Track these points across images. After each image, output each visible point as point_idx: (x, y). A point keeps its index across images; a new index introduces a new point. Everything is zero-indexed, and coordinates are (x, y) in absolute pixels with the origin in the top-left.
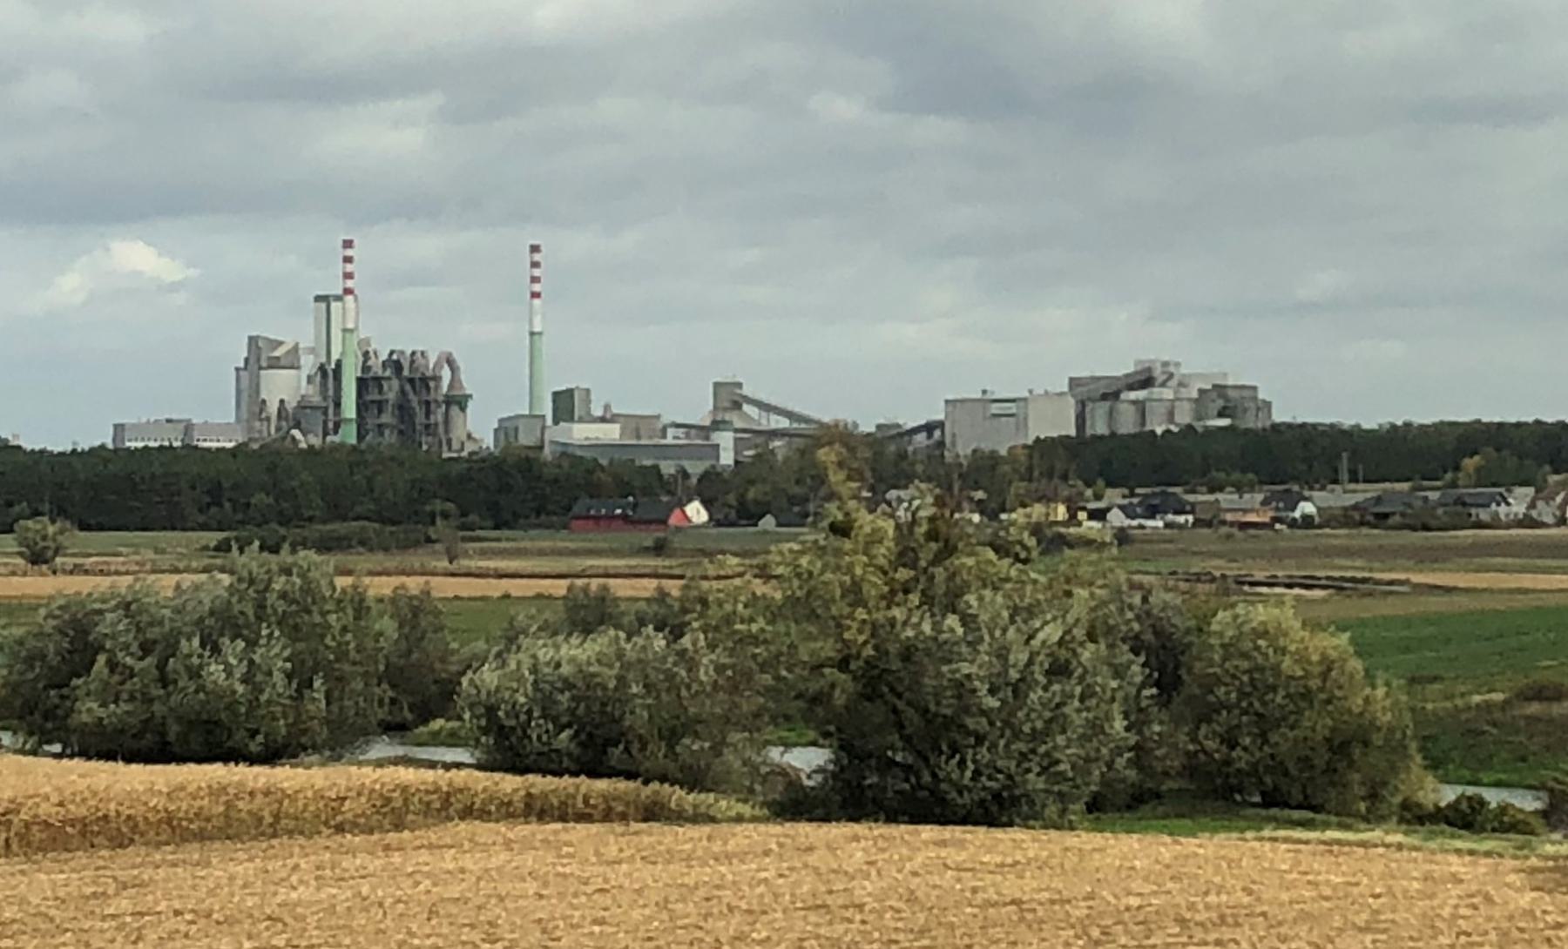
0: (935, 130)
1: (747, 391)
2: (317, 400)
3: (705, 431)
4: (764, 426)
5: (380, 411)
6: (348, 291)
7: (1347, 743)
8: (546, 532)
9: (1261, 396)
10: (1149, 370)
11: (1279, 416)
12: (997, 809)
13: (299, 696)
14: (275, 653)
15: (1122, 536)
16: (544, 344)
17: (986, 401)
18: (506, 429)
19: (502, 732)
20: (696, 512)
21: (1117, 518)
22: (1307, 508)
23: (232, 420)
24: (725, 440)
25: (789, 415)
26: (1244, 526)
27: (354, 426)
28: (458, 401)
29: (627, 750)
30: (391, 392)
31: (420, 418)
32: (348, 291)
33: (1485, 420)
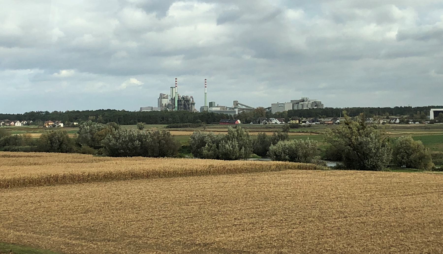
0: (262, 61)
1: (239, 102)
2: (171, 104)
3: (233, 109)
4: (241, 108)
6: (176, 86)
7: (422, 157)
12: (374, 168)
13: (240, 150)
14: (236, 143)
15: (309, 126)
16: (207, 95)
17: (278, 104)
18: (202, 108)
19: (276, 155)
20: (239, 121)
21: (307, 122)
22: (338, 121)
23: (157, 107)
24: (236, 110)
25: (246, 106)
26: (328, 124)
27: (177, 108)
28: (193, 104)
29: (298, 159)
30: (183, 102)
31: (187, 107)
32: (176, 86)
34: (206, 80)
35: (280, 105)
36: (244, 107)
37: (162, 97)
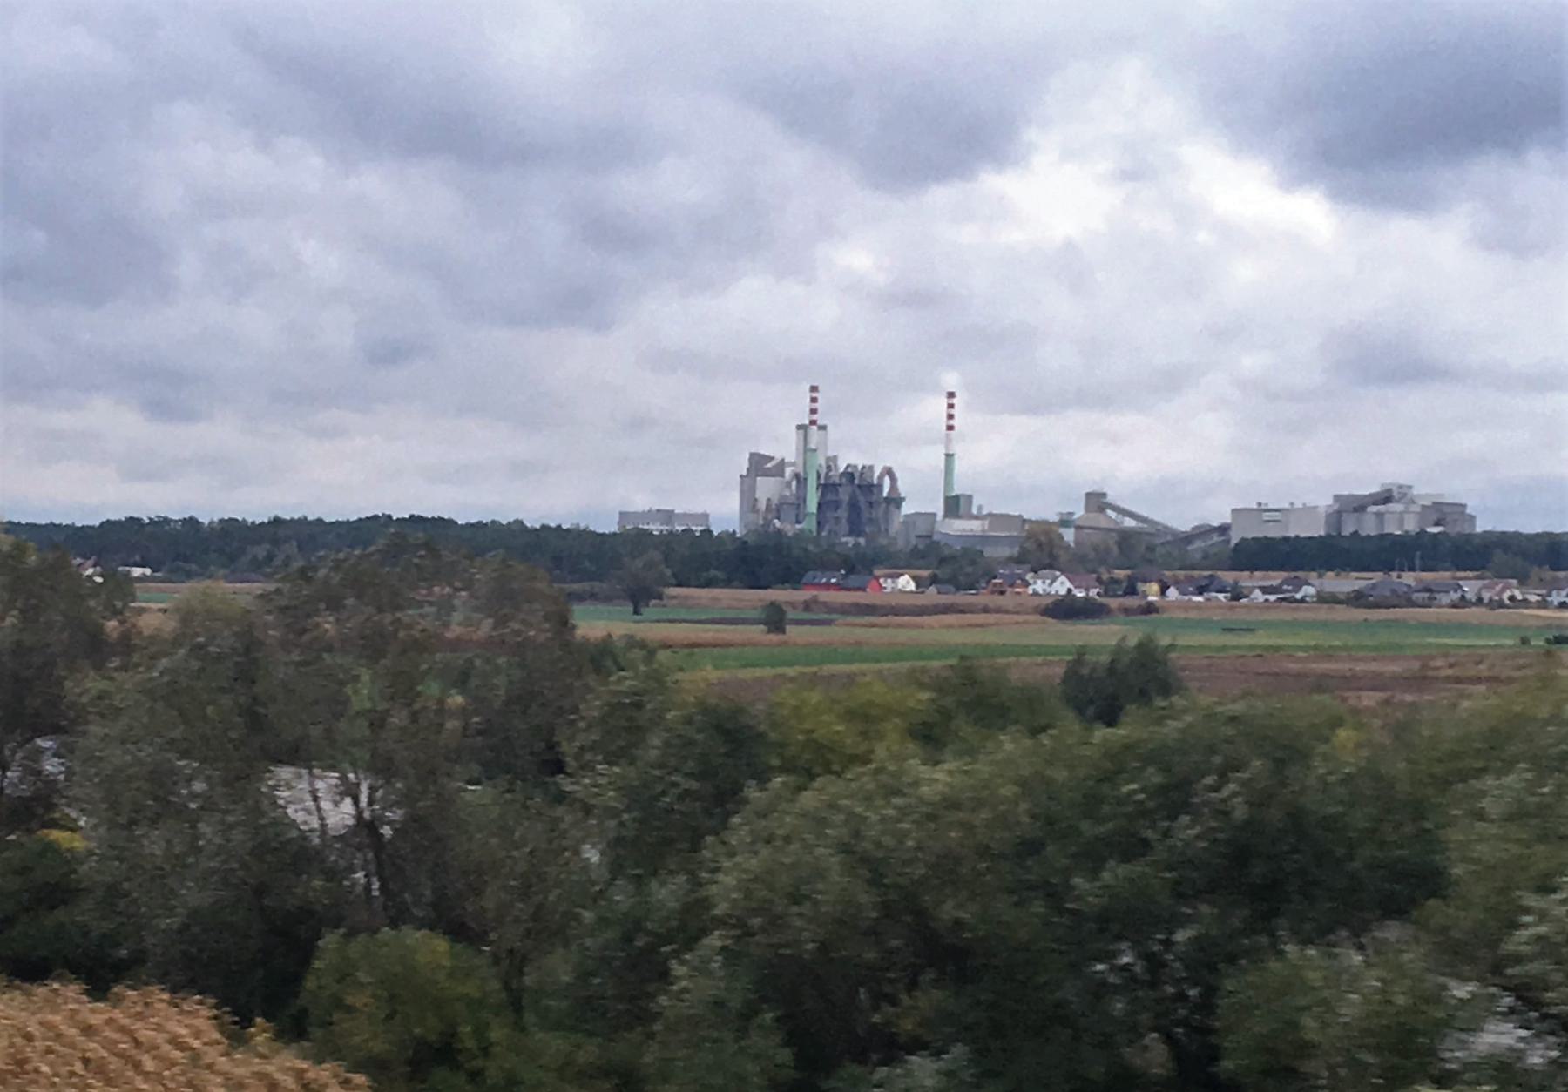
1: (1110, 499)
5: (837, 509)
6: (813, 422)
8: (602, 607)
9: (1468, 511)
10: (1389, 491)
11: (1480, 528)
30: (844, 495)
31: (865, 515)
33: (1302, 535)
34: (814, 389)
35: (1266, 516)
36: (1129, 523)
37: (759, 465)
